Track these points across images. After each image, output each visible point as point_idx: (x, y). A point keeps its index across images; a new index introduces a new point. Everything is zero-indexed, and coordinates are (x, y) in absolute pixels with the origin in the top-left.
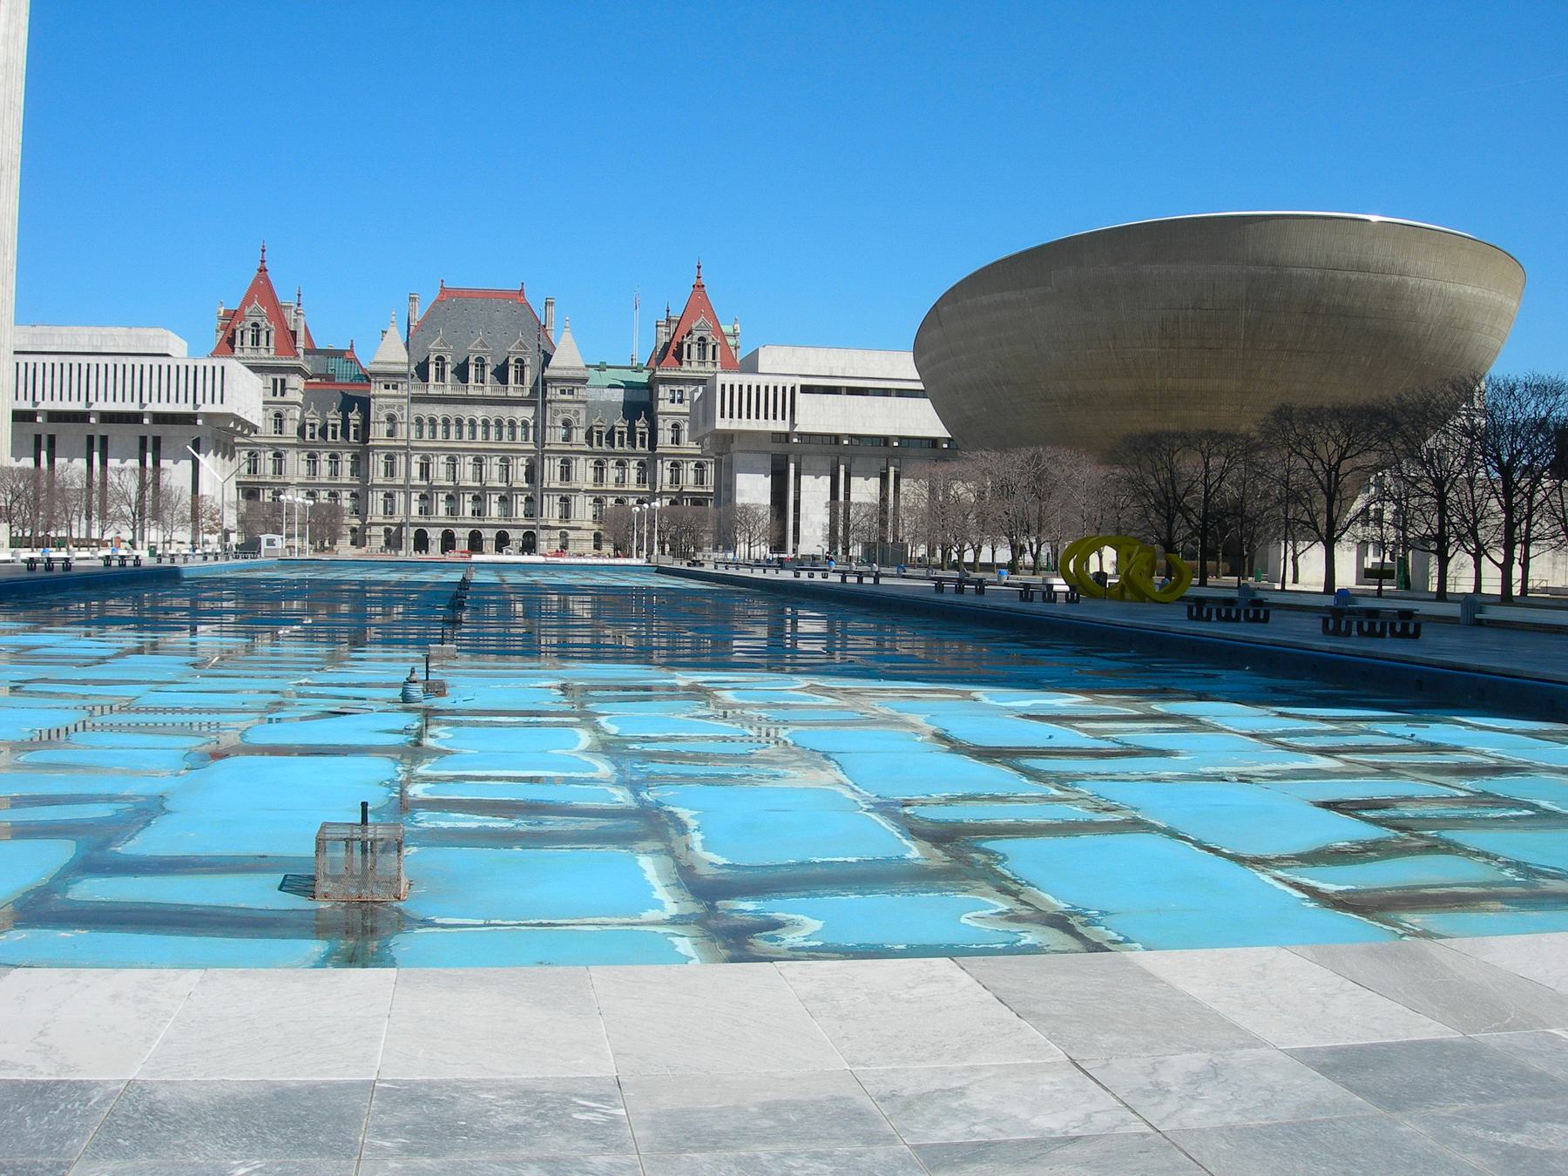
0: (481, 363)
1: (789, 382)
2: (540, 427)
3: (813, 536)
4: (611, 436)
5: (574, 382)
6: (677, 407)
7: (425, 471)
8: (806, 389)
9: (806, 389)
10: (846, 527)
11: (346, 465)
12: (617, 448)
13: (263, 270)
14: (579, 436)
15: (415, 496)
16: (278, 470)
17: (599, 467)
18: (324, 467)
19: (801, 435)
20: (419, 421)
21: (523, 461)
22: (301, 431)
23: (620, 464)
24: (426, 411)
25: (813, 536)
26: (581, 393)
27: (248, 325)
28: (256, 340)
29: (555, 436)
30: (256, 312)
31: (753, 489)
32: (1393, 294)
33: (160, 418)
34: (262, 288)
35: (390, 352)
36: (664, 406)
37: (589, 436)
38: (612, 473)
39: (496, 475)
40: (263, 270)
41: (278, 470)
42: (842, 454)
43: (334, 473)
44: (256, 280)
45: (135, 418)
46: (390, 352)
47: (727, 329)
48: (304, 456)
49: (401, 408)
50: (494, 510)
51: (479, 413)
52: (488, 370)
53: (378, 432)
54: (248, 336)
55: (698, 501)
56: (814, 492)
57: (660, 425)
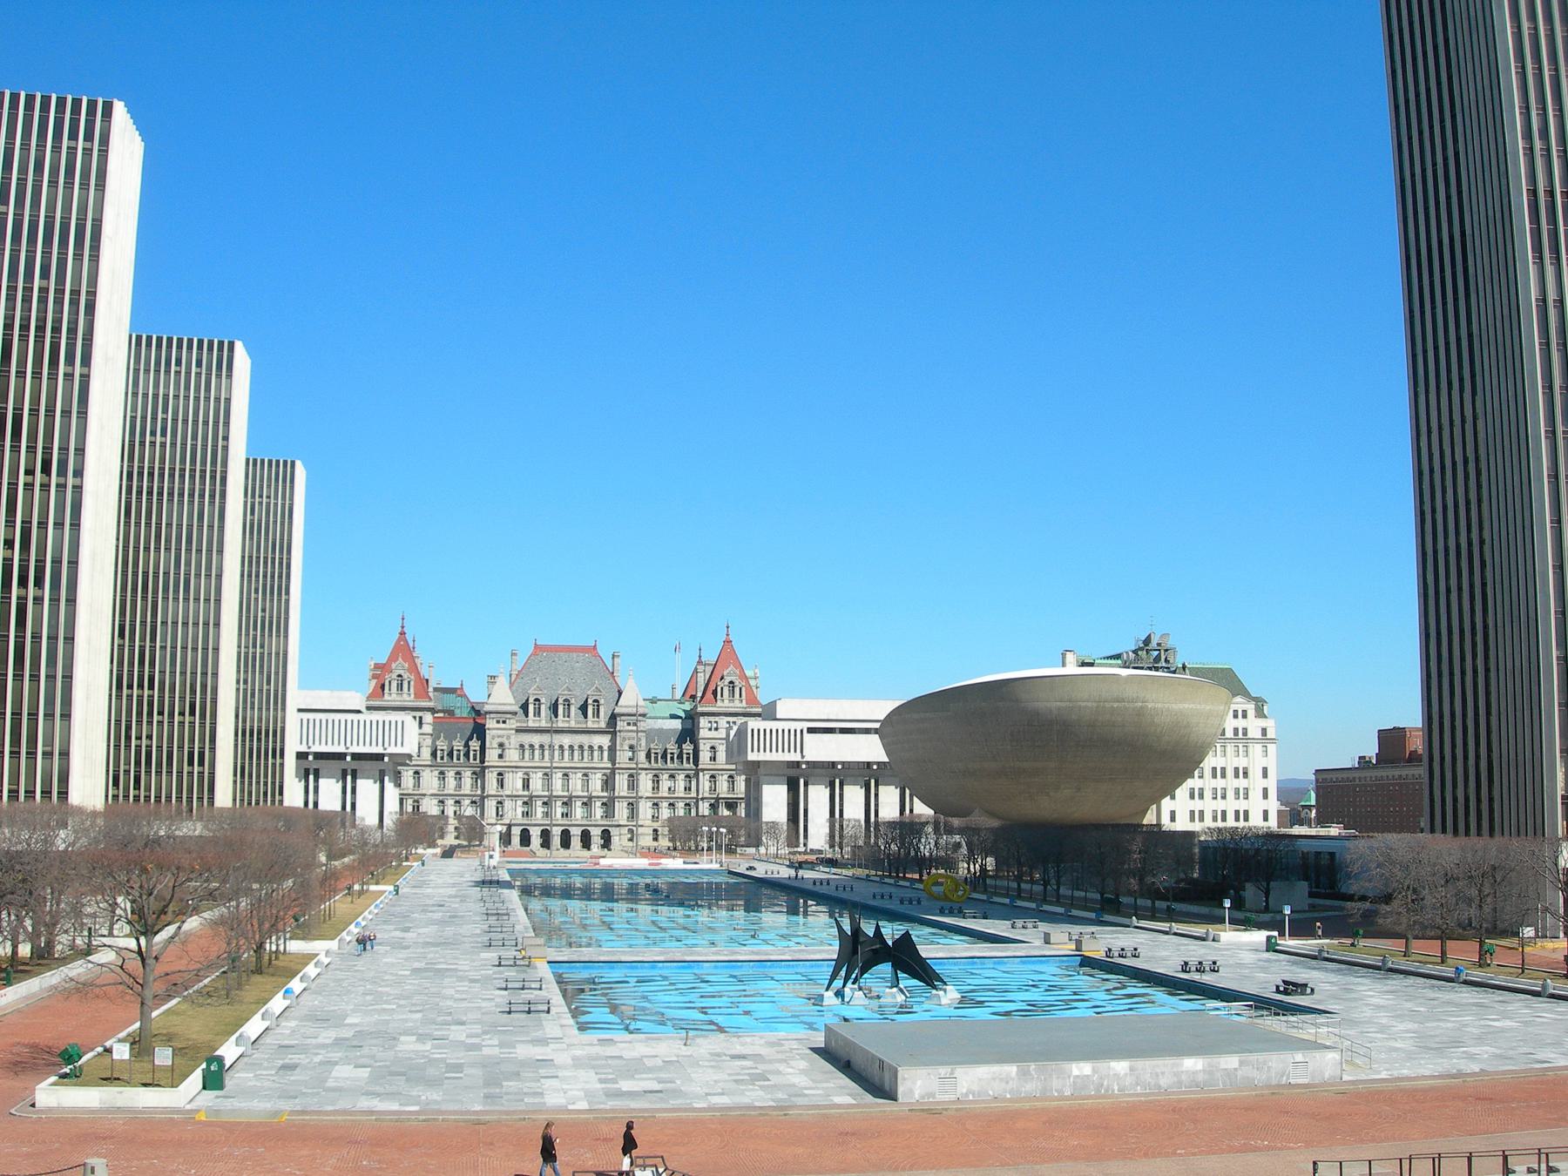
0: (568, 703)
1: (799, 726)
2: (612, 750)
3: (818, 835)
4: (664, 756)
5: (637, 716)
6: (713, 734)
7: (526, 785)
8: (810, 730)
9: (811, 730)
10: (841, 836)
11: (467, 781)
12: (670, 765)
13: (403, 633)
14: (642, 756)
15: (520, 803)
16: (417, 784)
17: (656, 780)
18: (451, 782)
19: (807, 763)
20: (522, 746)
21: (599, 776)
22: (434, 754)
23: (672, 777)
24: (527, 739)
25: (818, 835)
26: (643, 725)
27: (394, 676)
28: (400, 687)
29: (623, 757)
30: (400, 667)
31: (774, 801)
32: (1140, 713)
33: (356, 756)
34: (403, 649)
35: (502, 697)
36: (703, 733)
37: (648, 756)
38: (665, 783)
39: (579, 787)
40: (403, 633)
41: (417, 784)
42: (835, 774)
43: (459, 786)
44: (399, 640)
45: (341, 756)
46: (502, 697)
47: (749, 673)
48: (436, 773)
49: (508, 737)
50: (579, 811)
51: (566, 740)
52: (573, 709)
53: (492, 755)
54: (394, 684)
55: (731, 805)
56: (818, 797)
57: (701, 747)
